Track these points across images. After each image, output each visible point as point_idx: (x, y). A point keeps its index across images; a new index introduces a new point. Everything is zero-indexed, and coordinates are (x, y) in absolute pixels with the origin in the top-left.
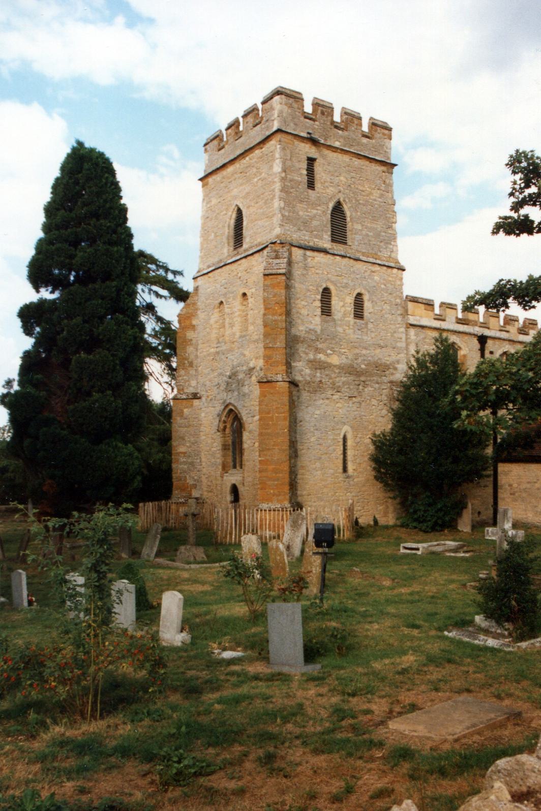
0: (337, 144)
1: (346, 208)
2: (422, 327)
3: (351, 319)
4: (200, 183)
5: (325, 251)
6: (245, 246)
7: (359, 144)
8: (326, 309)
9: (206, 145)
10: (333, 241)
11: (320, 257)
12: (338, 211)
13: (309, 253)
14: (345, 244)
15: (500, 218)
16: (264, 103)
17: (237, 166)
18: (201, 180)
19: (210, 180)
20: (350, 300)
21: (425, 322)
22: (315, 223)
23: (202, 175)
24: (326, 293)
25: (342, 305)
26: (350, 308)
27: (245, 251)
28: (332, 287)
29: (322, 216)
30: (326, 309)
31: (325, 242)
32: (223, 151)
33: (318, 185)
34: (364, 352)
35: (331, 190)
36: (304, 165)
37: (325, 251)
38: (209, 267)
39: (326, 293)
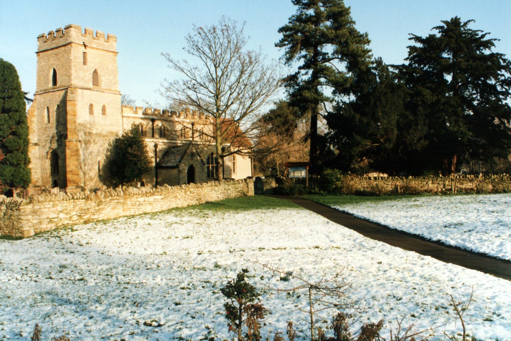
0: (95, 46)
1: (98, 71)
2: (128, 117)
3: (101, 115)
4: (36, 54)
5: (90, 89)
6: (58, 85)
7: (104, 45)
8: (91, 112)
9: (38, 38)
10: (94, 85)
11: (88, 92)
12: (95, 72)
13: (84, 91)
14: (98, 85)
15: (281, 30)
16: (65, 29)
17: (53, 51)
18: (37, 53)
19: (41, 54)
20: (101, 108)
21: (129, 115)
22: (87, 78)
23: (37, 51)
24: (91, 105)
25: (97, 110)
26: (101, 112)
27: (58, 88)
28: (93, 104)
29: (89, 76)
30: (91, 112)
31: (91, 85)
32: (46, 43)
33: (88, 63)
34: (106, 128)
35: (92, 65)
36: (82, 56)
37: (90, 89)
38: (41, 91)
39: (91, 105)
